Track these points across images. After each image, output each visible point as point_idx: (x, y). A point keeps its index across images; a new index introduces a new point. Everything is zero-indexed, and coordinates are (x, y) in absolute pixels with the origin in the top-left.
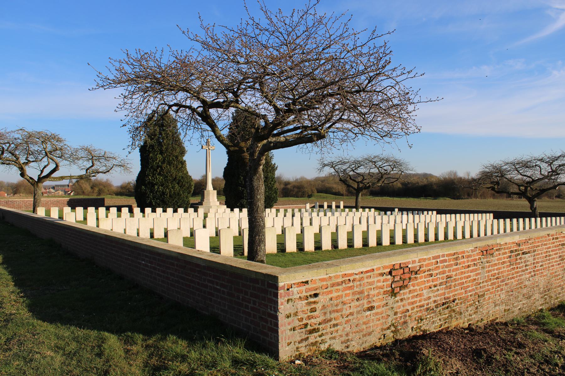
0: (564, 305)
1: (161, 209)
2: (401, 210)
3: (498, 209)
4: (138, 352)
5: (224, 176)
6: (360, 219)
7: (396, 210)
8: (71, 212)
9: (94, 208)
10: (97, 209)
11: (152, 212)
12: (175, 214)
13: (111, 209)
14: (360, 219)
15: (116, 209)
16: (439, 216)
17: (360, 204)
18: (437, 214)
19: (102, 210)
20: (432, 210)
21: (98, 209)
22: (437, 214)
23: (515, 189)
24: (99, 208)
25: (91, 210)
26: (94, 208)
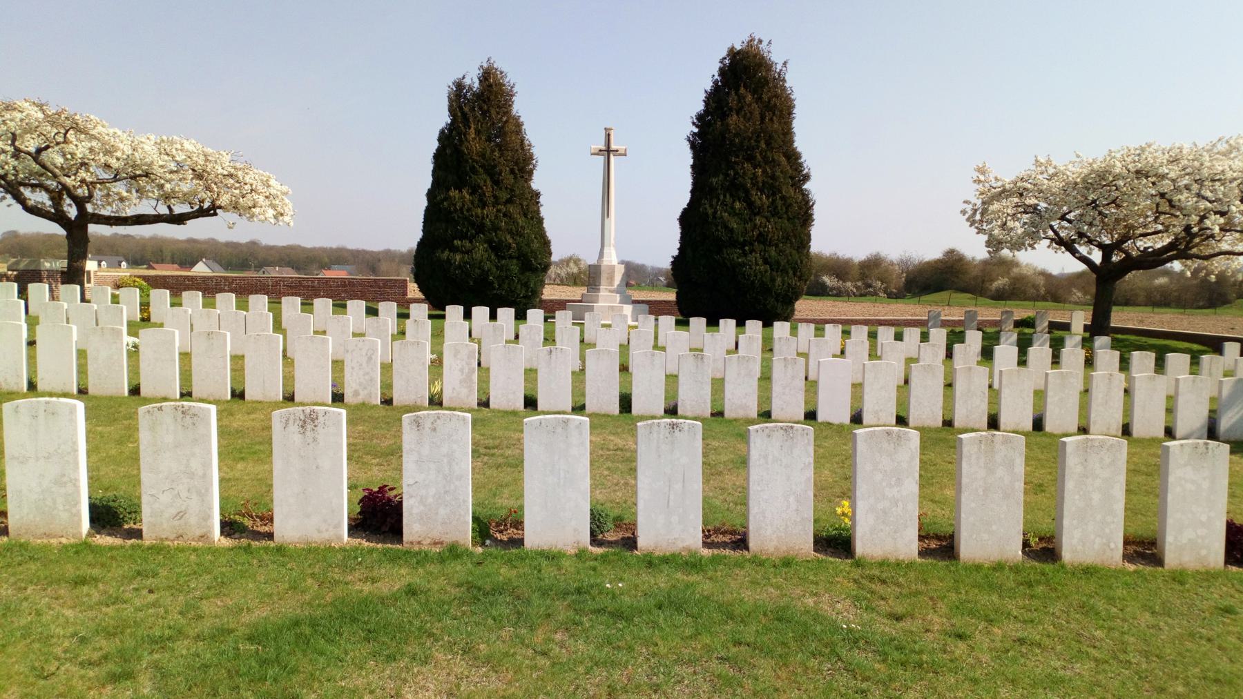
1: (512, 311)
9: (760, 323)
26: (760, 323)
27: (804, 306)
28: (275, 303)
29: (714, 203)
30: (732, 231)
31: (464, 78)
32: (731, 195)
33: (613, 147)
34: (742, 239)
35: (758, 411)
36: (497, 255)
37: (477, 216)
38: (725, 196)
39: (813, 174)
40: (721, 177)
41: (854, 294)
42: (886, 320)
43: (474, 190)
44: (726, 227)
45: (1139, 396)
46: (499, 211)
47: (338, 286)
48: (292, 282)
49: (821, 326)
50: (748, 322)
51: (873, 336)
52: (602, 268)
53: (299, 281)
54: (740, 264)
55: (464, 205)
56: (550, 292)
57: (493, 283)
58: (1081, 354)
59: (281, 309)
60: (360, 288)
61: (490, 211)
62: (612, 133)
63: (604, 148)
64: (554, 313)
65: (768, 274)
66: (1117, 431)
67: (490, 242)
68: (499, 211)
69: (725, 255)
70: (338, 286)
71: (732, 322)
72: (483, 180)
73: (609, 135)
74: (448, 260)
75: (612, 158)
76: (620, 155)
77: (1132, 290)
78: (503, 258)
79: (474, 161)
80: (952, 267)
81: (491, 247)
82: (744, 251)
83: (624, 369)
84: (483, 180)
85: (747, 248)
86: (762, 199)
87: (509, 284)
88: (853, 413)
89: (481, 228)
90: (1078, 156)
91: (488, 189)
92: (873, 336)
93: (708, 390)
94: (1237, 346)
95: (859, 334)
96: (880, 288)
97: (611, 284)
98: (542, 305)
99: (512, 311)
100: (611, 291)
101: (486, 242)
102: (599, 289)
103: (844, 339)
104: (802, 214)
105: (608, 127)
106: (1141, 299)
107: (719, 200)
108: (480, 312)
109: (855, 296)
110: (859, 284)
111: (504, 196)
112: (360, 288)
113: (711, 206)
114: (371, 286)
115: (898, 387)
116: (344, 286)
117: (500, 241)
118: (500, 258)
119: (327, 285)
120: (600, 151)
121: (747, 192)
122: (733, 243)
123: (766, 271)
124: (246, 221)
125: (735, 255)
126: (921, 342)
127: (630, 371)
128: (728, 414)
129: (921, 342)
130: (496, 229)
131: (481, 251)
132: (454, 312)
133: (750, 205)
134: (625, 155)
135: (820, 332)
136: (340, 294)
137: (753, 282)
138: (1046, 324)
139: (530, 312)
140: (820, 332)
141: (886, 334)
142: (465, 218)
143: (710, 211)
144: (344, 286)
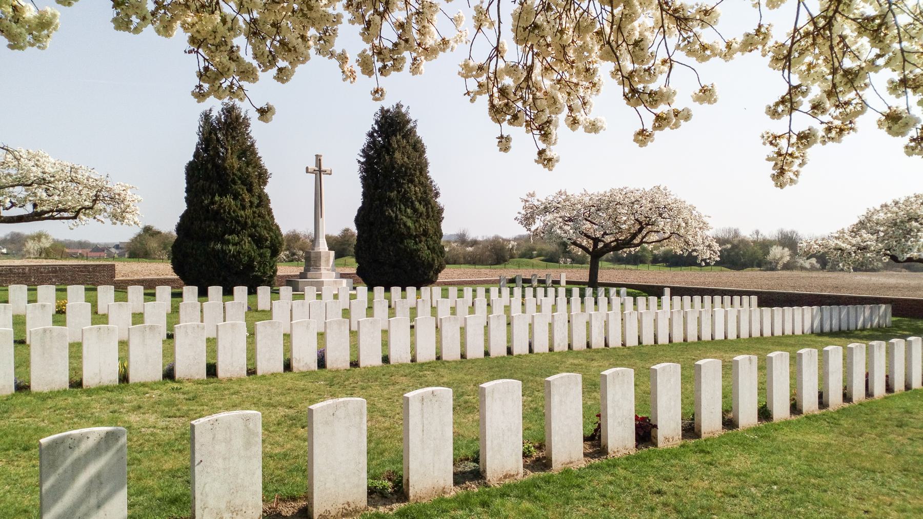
0: (767, 1)
1: (245, 289)
2: (677, 291)
3: (821, 291)
4: (81, 195)
5: (180, 228)
6: (551, 325)
7: (667, 291)
8: (770, 66)
9: (383, 288)
10: (387, 290)
11: (295, 297)
12: (77, 339)
13: (131, 289)
14: (551, 325)
15: (141, 289)
16: (767, 311)
17: (603, 277)
18: (760, 304)
19: (106, 293)
20: (749, 293)
21: (597, 290)
22: (760, 304)
23: (660, 259)
24: (375, 288)
25: (76, 292)
26: (383, 288)
27: (448, 274)
29: (395, 209)
30: (409, 228)
31: (210, 110)
32: (404, 206)
33: (323, 168)
34: (415, 233)
35: (70, 379)
36: (257, 245)
37: (242, 216)
41: (284, 260)
43: (236, 196)
46: (254, 212)
47: (49, 272)
51: (487, 291)
53: (10, 269)
54: (415, 250)
55: (231, 209)
57: (256, 267)
59: (97, 296)
60: (70, 273)
61: (249, 212)
62: (322, 159)
64: (154, 288)
65: (431, 256)
66: (241, 369)
67: (251, 236)
68: (254, 212)
69: (406, 244)
70: (49, 272)
72: (239, 187)
74: (223, 251)
77: (457, 254)
78: (262, 248)
79: (234, 174)
81: (254, 240)
82: (416, 241)
83: (20, 342)
84: (239, 187)
85: (417, 239)
86: (422, 208)
87: (263, 267)
88: (166, 367)
89: (244, 226)
90: (585, 191)
91: (247, 197)
92: (487, 291)
93: (203, 346)
95: (481, 290)
96: (302, 256)
99: (245, 289)
100: (328, 270)
103: (272, 299)
104: (436, 215)
105: (319, 154)
107: (397, 207)
108: (396, 291)
109: (286, 262)
112: (70, 273)
113: (393, 211)
114: (81, 271)
115: (163, 341)
116: (53, 272)
117: (260, 235)
118: (259, 248)
120: (315, 170)
121: (412, 203)
122: (410, 236)
123: (429, 254)
125: (411, 244)
126: (145, 302)
127: (28, 342)
129: (145, 302)
130: (254, 226)
131: (247, 245)
132: (379, 291)
133: (415, 210)
134: (330, 174)
135: (150, 296)
137: (424, 261)
138: (551, 281)
139: (237, 289)
140: (150, 296)
141: (494, 290)
142: (232, 218)
143: (394, 215)
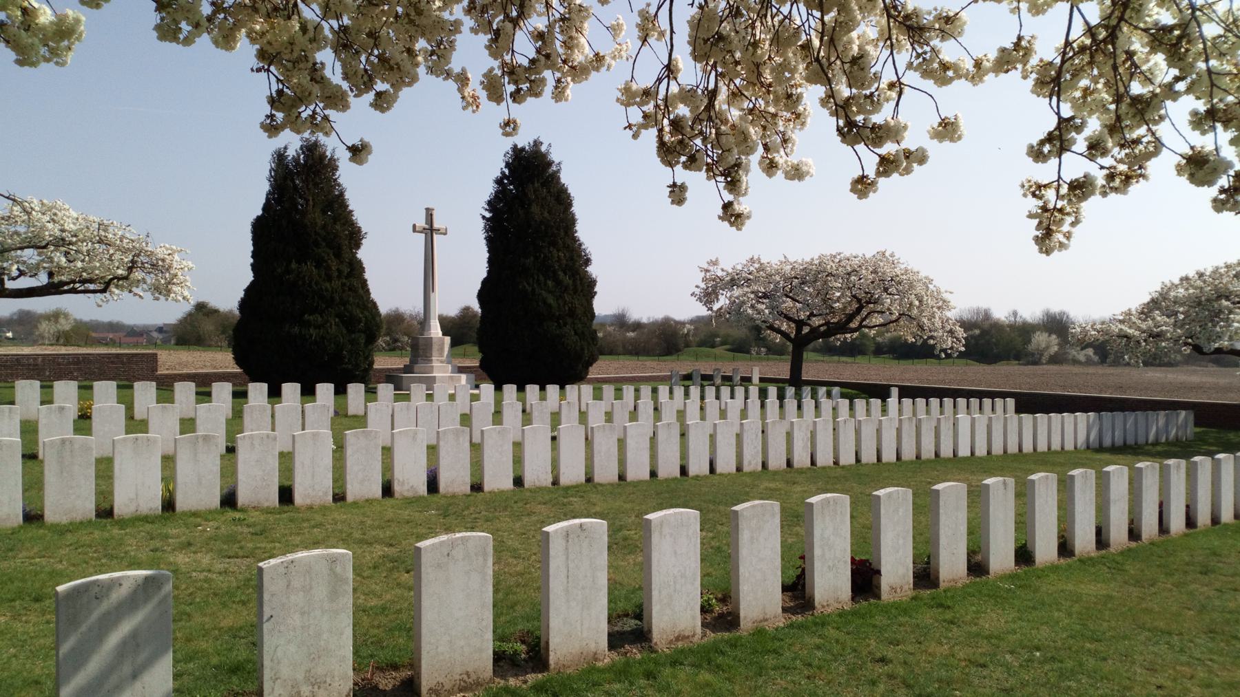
1: (331, 387)
26: (558, 386)
28: (125, 388)
30: (550, 306)
31: (286, 148)
33: (436, 226)
34: (557, 314)
37: (327, 290)
38: (538, 276)
39: (593, 257)
40: (532, 258)
41: (383, 348)
42: (224, 373)
43: (319, 263)
44: (545, 302)
45: (770, 431)
46: (343, 285)
48: (6, 361)
49: (48, 383)
50: (548, 386)
52: (434, 341)
53: (17, 359)
56: (382, 362)
58: (758, 403)
61: (336, 284)
63: (427, 227)
64: (210, 385)
68: (343, 285)
70: (69, 363)
71: (537, 387)
73: (431, 215)
75: (435, 236)
76: (441, 234)
80: (468, 323)
88: (225, 491)
90: (785, 257)
91: (334, 265)
93: (274, 463)
94: (897, 389)
97: (441, 355)
98: (590, 381)
99: (331, 387)
100: (442, 362)
101: (337, 316)
102: (431, 361)
106: (620, 349)
107: (534, 279)
109: (386, 350)
110: (388, 338)
111: (346, 270)
114: (112, 362)
116: (74, 363)
119: (54, 362)
120: (424, 229)
124: (148, 296)
127: (41, 457)
128: (50, 516)
134: (445, 234)
135: (204, 395)
136: (71, 373)
140: (204, 395)
141: (663, 390)
143: (530, 289)
144: (74, 363)
